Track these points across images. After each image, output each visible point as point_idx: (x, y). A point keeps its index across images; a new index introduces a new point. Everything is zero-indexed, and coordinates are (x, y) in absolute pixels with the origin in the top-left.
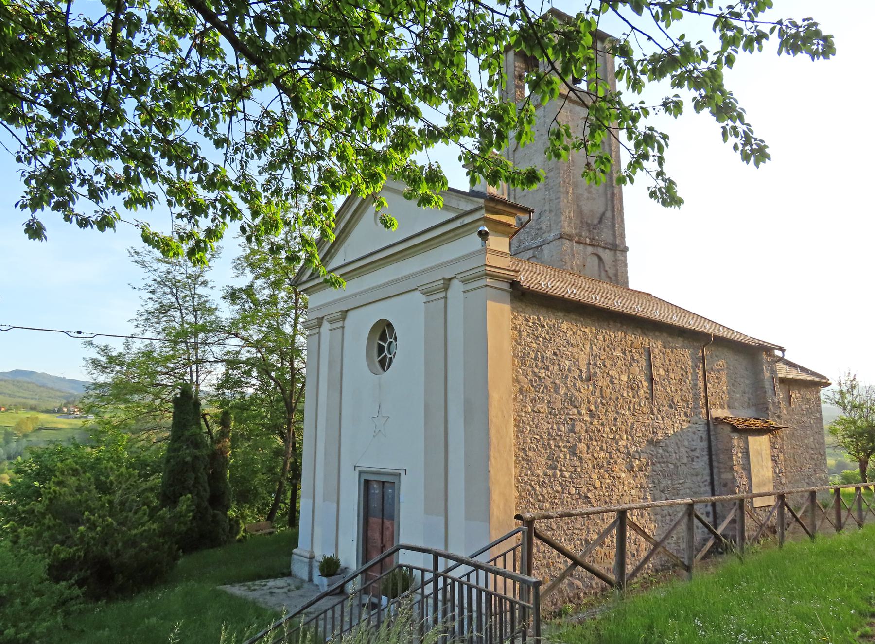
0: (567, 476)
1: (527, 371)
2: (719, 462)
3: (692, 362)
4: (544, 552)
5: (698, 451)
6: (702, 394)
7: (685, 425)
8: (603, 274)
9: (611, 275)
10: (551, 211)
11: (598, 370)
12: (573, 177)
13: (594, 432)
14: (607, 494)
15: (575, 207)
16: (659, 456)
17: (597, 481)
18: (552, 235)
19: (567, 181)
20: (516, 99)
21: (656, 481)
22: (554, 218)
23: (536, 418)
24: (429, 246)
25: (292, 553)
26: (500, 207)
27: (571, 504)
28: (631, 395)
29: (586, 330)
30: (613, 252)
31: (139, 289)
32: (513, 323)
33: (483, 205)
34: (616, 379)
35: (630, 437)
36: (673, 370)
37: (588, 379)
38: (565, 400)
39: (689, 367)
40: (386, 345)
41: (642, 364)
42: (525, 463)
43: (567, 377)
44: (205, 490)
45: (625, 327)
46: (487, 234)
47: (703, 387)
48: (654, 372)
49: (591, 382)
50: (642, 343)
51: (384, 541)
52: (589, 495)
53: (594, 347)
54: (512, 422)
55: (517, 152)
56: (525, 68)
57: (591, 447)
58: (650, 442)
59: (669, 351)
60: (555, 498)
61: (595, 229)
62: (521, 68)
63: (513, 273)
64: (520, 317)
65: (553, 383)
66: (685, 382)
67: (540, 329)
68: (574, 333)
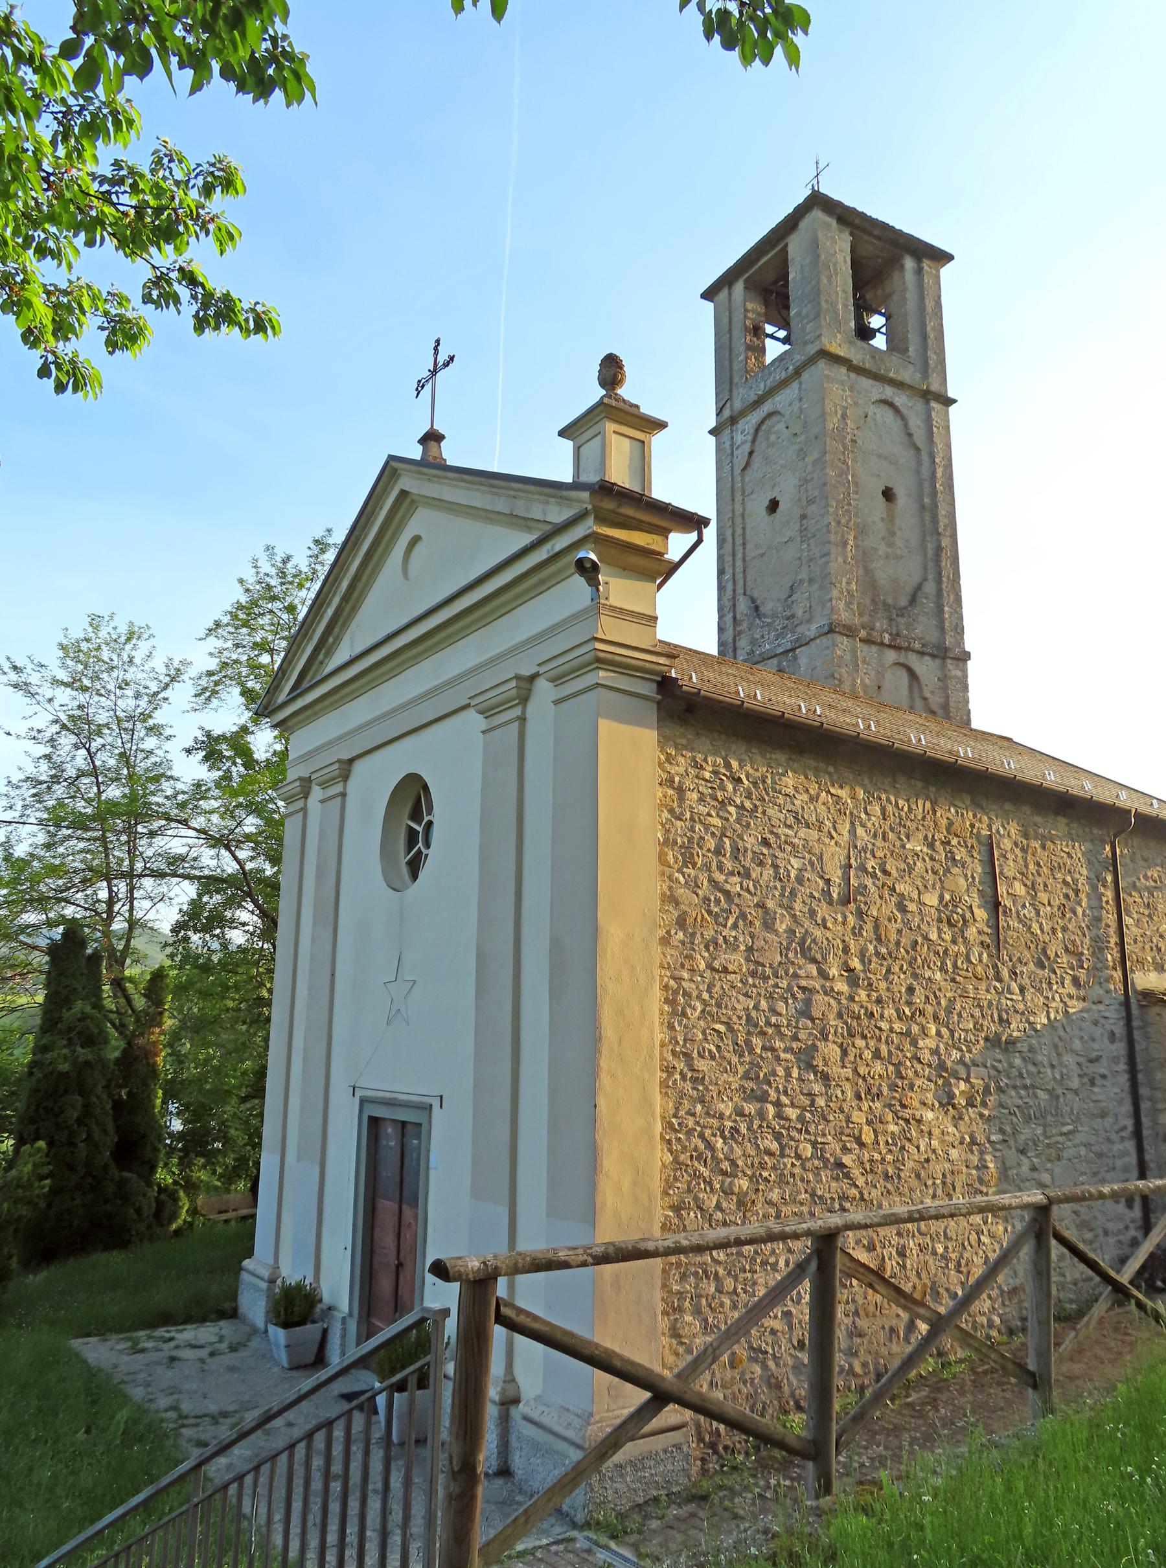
0: (794, 1117)
1: (696, 877)
2: (1153, 1088)
3: (1089, 870)
4: (735, 1292)
5: (1104, 1061)
6: (1114, 939)
7: (1075, 1006)
8: (919, 703)
9: (935, 707)
10: (811, 581)
11: (869, 882)
12: (856, 515)
13: (858, 1018)
14: (889, 1157)
15: (861, 572)
16: (1014, 1072)
17: (866, 1128)
18: (814, 626)
19: (843, 521)
20: (747, 372)
21: (1008, 1129)
22: (816, 595)
23: (718, 984)
24: (493, 611)
25: (241, 1269)
26: (628, 511)
27: (802, 1180)
28: (948, 937)
29: (843, 793)
30: (938, 661)
31: (18, 736)
32: (664, 770)
33: (589, 507)
34: (912, 900)
35: (944, 1031)
36: (1046, 885)
37: (846, 900)
38: (790, 944)
39: (1082, 880)
40: (420, 829)
41: (973, 871)
42: (688, 1086)
43: (793, 893)
44: (105, 1131)
45: (933, 789)
46: (595, 567)
47: (1114, 925)
48: (1002, 889)
49: (852, 906)
50: (972, 826)
51: (402, 1254)
52: (847, 1160)
53: (860, 831)
54: (657, 993)
55: (749, 471)
56: (766, 315)
57: (852, 1052)
58: (993, 1042)
59: (1036, 844)
60: (763, 1166)
61: (902, 615)
62: (759, 314)
63: (662, 660)
64: (681, 759)
65: (761, 906)
66: (1075, 913)
67: (730, 787)
68: (812, 799)
